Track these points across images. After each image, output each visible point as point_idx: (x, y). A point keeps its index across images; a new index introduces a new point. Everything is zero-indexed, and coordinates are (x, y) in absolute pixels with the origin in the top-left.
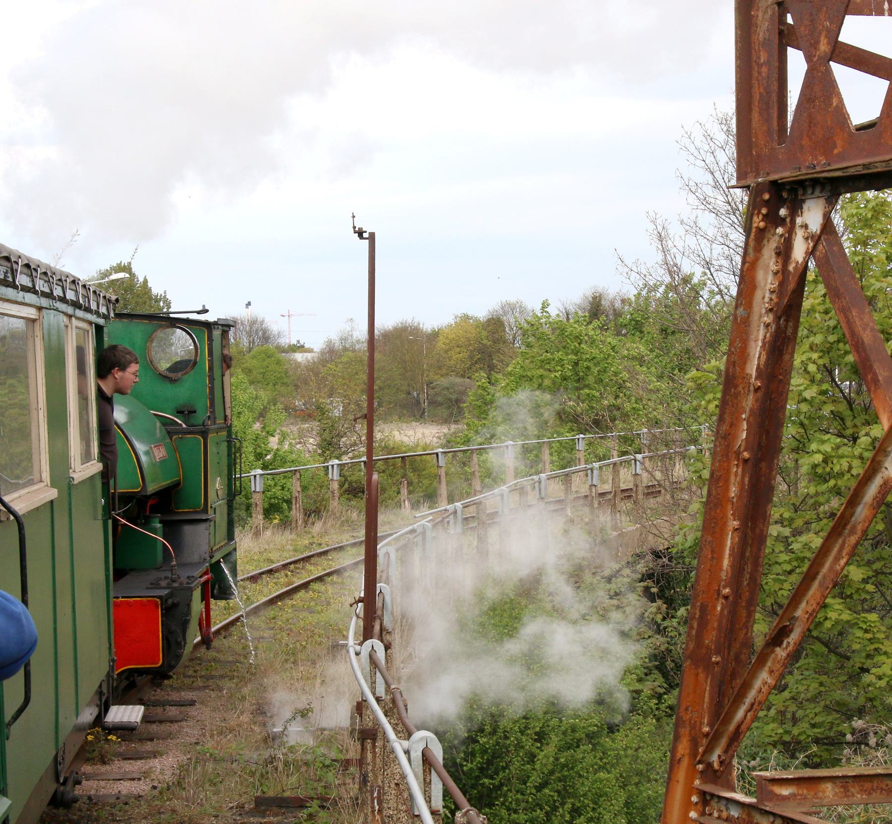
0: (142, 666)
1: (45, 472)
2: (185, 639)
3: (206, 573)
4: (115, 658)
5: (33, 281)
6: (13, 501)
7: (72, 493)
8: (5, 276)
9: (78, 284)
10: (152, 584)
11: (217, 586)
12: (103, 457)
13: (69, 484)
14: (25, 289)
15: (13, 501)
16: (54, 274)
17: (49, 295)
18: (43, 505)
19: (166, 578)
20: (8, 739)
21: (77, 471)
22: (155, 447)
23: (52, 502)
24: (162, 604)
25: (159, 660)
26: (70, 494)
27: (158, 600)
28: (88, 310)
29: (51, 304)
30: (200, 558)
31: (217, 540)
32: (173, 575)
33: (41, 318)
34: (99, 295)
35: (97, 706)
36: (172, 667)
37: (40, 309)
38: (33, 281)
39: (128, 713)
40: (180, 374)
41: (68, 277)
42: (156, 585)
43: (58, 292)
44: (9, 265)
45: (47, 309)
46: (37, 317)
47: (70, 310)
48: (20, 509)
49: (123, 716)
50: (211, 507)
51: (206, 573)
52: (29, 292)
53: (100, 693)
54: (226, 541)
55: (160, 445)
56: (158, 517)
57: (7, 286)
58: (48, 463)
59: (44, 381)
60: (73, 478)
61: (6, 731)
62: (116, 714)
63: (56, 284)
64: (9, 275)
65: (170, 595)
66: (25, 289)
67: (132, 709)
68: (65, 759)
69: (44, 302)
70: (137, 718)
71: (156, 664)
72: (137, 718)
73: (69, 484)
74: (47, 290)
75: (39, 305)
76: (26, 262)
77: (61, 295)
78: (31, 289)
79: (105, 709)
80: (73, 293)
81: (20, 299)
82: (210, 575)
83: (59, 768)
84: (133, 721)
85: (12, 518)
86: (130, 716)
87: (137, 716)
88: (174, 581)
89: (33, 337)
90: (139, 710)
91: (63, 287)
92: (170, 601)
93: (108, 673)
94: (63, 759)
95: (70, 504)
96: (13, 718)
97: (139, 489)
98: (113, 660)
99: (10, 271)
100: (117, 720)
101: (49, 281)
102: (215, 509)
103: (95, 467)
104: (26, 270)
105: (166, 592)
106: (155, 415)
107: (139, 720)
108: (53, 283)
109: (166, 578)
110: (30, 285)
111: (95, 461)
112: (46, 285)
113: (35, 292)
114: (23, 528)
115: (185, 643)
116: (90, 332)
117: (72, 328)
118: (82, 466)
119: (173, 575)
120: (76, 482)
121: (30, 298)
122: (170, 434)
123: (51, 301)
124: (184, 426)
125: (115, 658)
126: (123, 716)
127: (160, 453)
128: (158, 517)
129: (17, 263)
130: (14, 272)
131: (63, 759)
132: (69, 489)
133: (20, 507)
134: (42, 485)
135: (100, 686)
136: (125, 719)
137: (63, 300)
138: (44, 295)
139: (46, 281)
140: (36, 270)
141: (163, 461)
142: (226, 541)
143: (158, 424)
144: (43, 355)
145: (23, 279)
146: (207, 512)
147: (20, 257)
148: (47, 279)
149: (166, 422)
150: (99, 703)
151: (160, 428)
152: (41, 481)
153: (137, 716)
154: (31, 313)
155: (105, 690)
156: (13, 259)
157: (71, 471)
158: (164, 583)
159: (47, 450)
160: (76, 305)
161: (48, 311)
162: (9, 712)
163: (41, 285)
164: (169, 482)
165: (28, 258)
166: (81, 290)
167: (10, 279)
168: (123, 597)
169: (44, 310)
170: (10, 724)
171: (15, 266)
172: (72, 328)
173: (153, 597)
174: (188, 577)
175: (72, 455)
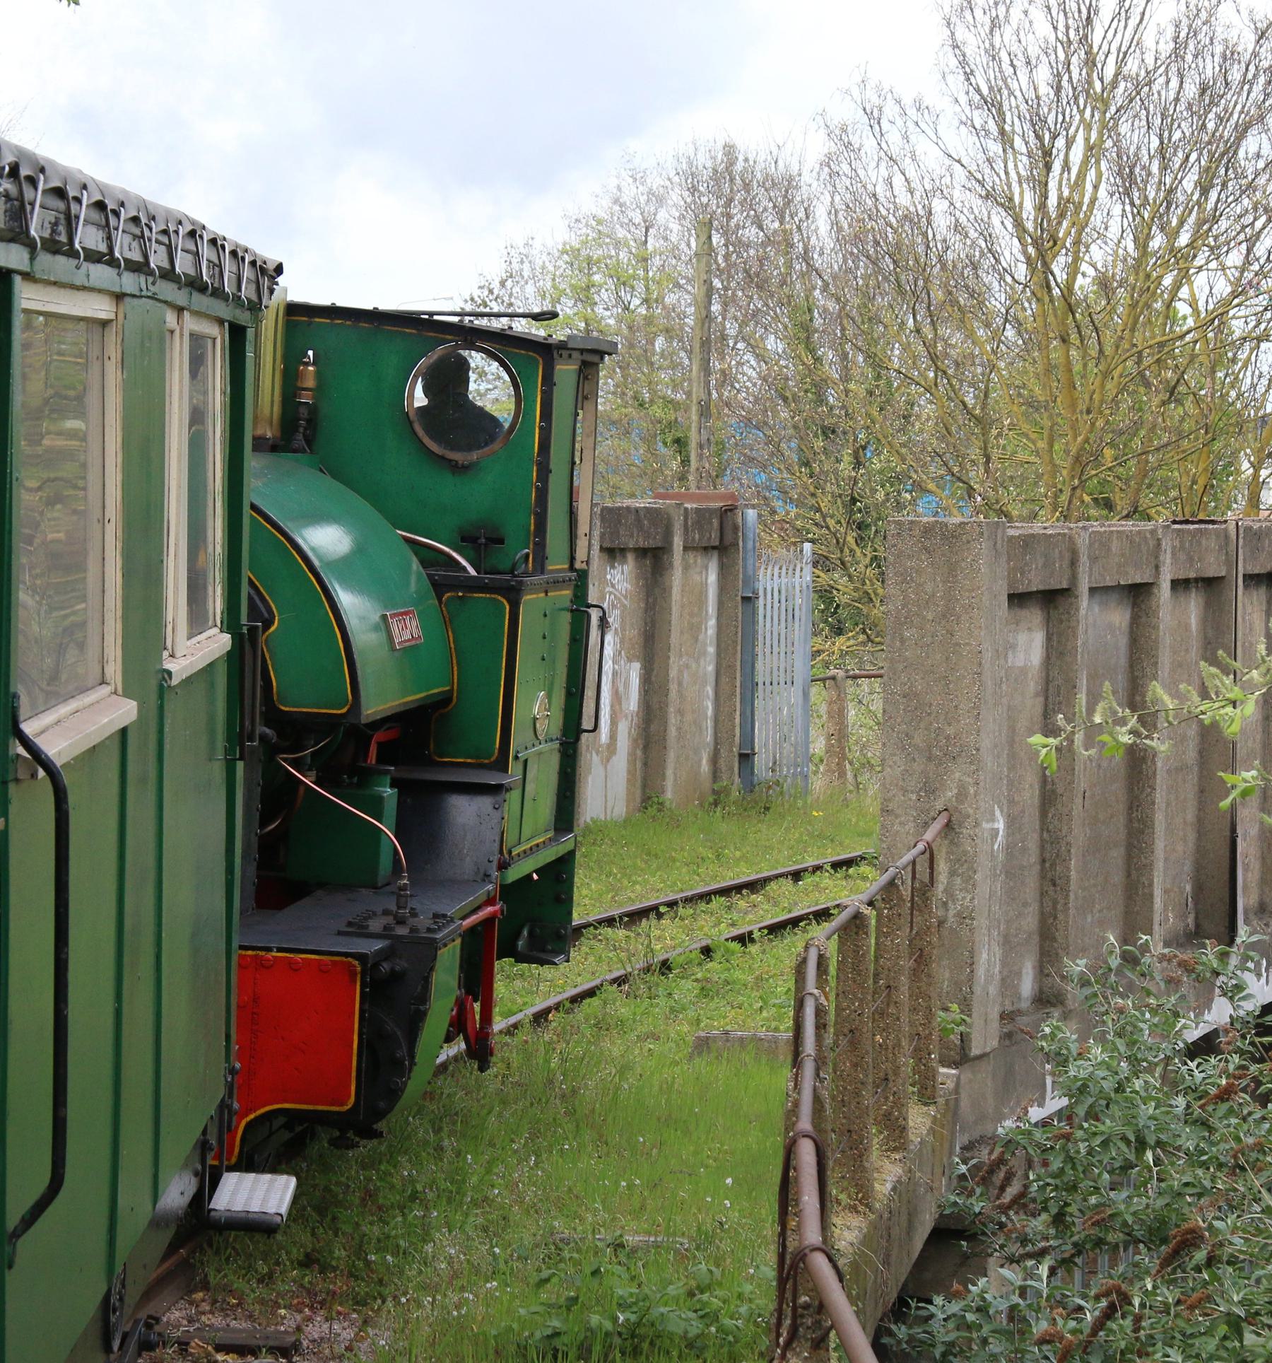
0: (310, 1107)
1: (112, 664)
2: (412, 1056)
3: (490, 901)
4: (238, 1065)
5: (109, 238)
6: (42, 732)
7: (166, 707)
8: (53, 231)
9: (201, 237)
10: (350, 924)
11: (525, 933)
12: (231, 624)
13: (161, 686)
14: (94, 257)
15: (42, 732)
16: (154, 218)
17: (140, 267)
18: (107, 739)
19: (386, 912)
20: (10, 1267)
21: (178, 654)
22: (393, 616)
23: (124, 732)
24: (363, 973)
25: (349, 1096)
26: (161, 708)
27: (356, 963)
28: (218, 293)
29: (144, 287)
30: (477, 873)
31: (527, 832)
32: (399, 908)
33: (121, 316)
34: (243, 259)
35: (196, 1174)
36: (381, 1115)
37: (119, 297)
38: (109, 238)
39: (260, 1193)
40: (474, 456)
41: (180, 223)
42: (358, 929)
43: (158, 259)
44: (61, 205)
45: (134, 296)
46: (112, 316)
47: (180, 297)
48: (59, 753)
49: (250, 1198)
50: (516, 758)
51: (490, 901)
52: (99, 261)
53: (203, 1146)
54: (551, 834)
55: (406, 613)
56: (388, 772)
57: (56, 252)
58: (119, 642)
59: (120, 460)
60: (170, 673)
61: (8, 1249)
62: (235, 1193)
63: (157, 242)
64: (61, 228)
65: (386, 954)
66: (94, 257)
67: (271, 1182)
68: (127, 1299)
69: (129, 282)
70: (279, 1206)
71: (342, 1105)
72: (279, 1206)
73: (161, 686)
74: (136, 256)
75: (117, 289)
76: (98, 197)
77: (166, 265)
78: (105, 255)
79: (209, 1182)
80: (190, 257)
81: (79, 280)
82: (497, 907)
83: (113, 1319)
84: (272, 1210)
85: (41, 773)
86: (265, 1200)
87: (281, 1200)
88: (401, 922)
89: (102, 358)
90: (286, 1187)
91: (169, 247)
92: (385, 967)
93: (223, 1100)
94: (121, 1299)
95: (161, 731)
96: (23, 1220)
97: (344, 710)
98: (232, 1071)
99: (63, 221)
100: (238, 1206)
101: (143, 236)
102: (526, 761)
103: (216, 643)
104: (96, 216)
105: (378, 945)
106: (406, 540)
107: (284, 1210)
108: (150, 240)
109: (386, 912)
110: (103, 248)
111: (216, 630)
112: (135, 244)
113: (113, 262)
114: (66, 797)
115: (413, 1063)
116: (218, 341)
117: (182, 335)
118: (189, 643)
119: (399, 908)
120: (175, 682)
121: (100, 274)
122: (439, 587)
123: (143, 279)
124: (472, 572)
125: (238, 1065)
126: (250, 1198)
127: (407, 631)
128: (388, 772)
129: (78, 200)
130: (70, 221)
131: (121, 1299)
132: (161, 697)
133: (57, 748)
134: (105, 690)
135: (204, 1132)
136: (255, 1207)
137: (168, 274)
138: (133, 267)
139: (135, 237)
140: (116, 214)
141: (411, 650)
142: (551, 834)
143: (415, 565)
144: (120, 399)
145: (87, 237)
146: (505, 769)
147: (85, 187)
148: (137, 231)
149: (430, 559)
150: (200, 1167)
151: (418, 573)
152: (103, 682)
153: (281, 1200)
154: (101, 308)
155: (214, 1142)
156: (72, 193)
157: (165, 654)
158: (375, 925)
159: (119, 613)
160: (196, 285)
161: (136, 301)
162: (17, 1206)
163: (125, 248)
164: (422, 695)
165: (101, 188)
166: (207, 252)
167: (63, 238)
168: (280, 950)
169: (127, 300)
170: (17, 1234)
171: (74, 207)
172: (182, 335)
173: (346, 955)
174: (436, 916)
175: (170, 619)
